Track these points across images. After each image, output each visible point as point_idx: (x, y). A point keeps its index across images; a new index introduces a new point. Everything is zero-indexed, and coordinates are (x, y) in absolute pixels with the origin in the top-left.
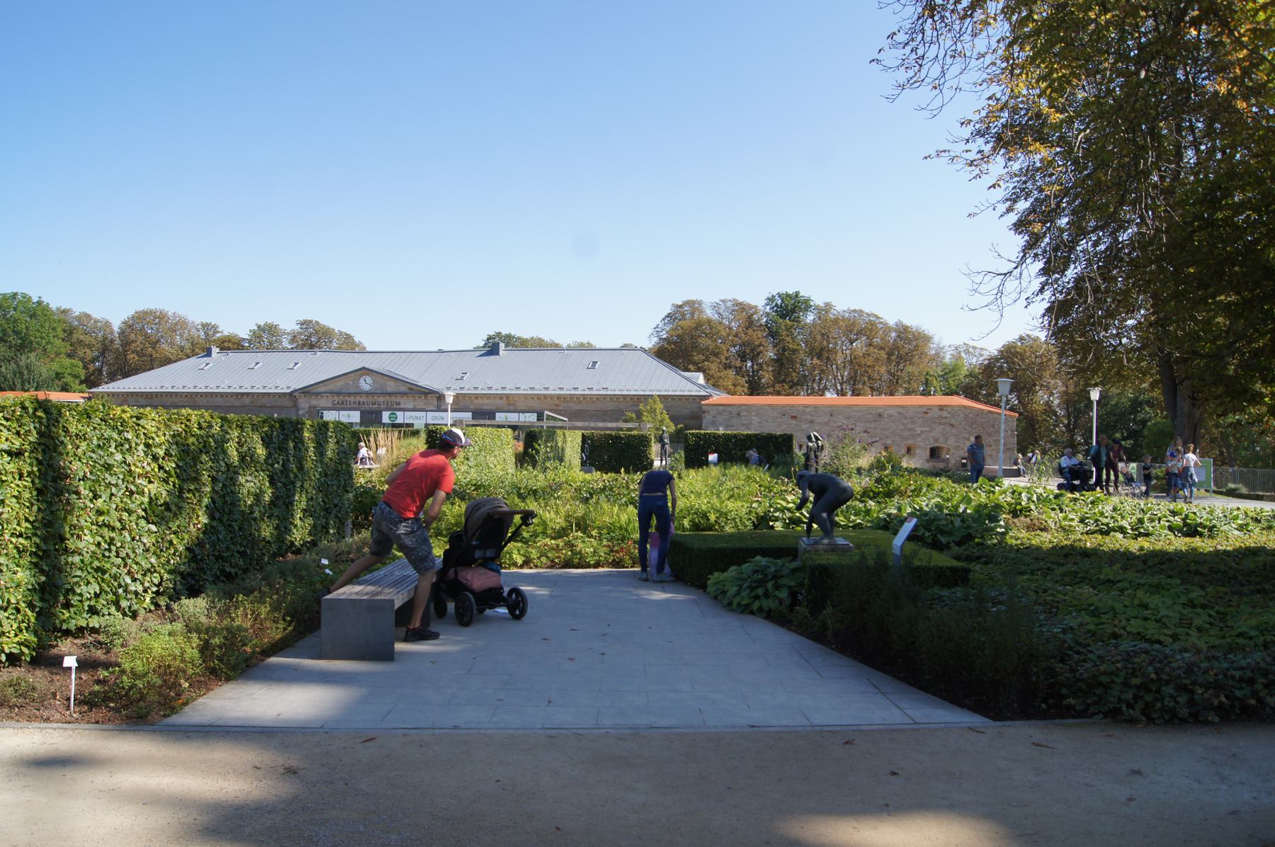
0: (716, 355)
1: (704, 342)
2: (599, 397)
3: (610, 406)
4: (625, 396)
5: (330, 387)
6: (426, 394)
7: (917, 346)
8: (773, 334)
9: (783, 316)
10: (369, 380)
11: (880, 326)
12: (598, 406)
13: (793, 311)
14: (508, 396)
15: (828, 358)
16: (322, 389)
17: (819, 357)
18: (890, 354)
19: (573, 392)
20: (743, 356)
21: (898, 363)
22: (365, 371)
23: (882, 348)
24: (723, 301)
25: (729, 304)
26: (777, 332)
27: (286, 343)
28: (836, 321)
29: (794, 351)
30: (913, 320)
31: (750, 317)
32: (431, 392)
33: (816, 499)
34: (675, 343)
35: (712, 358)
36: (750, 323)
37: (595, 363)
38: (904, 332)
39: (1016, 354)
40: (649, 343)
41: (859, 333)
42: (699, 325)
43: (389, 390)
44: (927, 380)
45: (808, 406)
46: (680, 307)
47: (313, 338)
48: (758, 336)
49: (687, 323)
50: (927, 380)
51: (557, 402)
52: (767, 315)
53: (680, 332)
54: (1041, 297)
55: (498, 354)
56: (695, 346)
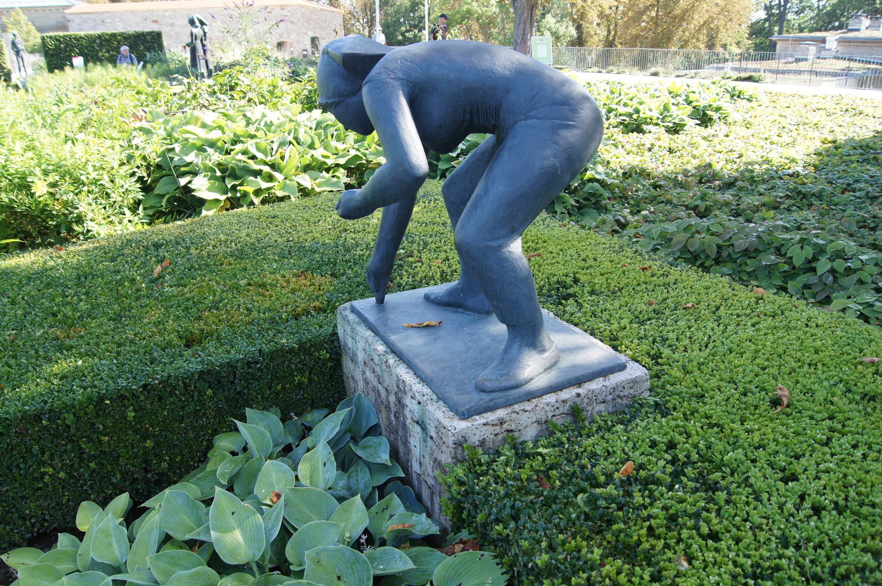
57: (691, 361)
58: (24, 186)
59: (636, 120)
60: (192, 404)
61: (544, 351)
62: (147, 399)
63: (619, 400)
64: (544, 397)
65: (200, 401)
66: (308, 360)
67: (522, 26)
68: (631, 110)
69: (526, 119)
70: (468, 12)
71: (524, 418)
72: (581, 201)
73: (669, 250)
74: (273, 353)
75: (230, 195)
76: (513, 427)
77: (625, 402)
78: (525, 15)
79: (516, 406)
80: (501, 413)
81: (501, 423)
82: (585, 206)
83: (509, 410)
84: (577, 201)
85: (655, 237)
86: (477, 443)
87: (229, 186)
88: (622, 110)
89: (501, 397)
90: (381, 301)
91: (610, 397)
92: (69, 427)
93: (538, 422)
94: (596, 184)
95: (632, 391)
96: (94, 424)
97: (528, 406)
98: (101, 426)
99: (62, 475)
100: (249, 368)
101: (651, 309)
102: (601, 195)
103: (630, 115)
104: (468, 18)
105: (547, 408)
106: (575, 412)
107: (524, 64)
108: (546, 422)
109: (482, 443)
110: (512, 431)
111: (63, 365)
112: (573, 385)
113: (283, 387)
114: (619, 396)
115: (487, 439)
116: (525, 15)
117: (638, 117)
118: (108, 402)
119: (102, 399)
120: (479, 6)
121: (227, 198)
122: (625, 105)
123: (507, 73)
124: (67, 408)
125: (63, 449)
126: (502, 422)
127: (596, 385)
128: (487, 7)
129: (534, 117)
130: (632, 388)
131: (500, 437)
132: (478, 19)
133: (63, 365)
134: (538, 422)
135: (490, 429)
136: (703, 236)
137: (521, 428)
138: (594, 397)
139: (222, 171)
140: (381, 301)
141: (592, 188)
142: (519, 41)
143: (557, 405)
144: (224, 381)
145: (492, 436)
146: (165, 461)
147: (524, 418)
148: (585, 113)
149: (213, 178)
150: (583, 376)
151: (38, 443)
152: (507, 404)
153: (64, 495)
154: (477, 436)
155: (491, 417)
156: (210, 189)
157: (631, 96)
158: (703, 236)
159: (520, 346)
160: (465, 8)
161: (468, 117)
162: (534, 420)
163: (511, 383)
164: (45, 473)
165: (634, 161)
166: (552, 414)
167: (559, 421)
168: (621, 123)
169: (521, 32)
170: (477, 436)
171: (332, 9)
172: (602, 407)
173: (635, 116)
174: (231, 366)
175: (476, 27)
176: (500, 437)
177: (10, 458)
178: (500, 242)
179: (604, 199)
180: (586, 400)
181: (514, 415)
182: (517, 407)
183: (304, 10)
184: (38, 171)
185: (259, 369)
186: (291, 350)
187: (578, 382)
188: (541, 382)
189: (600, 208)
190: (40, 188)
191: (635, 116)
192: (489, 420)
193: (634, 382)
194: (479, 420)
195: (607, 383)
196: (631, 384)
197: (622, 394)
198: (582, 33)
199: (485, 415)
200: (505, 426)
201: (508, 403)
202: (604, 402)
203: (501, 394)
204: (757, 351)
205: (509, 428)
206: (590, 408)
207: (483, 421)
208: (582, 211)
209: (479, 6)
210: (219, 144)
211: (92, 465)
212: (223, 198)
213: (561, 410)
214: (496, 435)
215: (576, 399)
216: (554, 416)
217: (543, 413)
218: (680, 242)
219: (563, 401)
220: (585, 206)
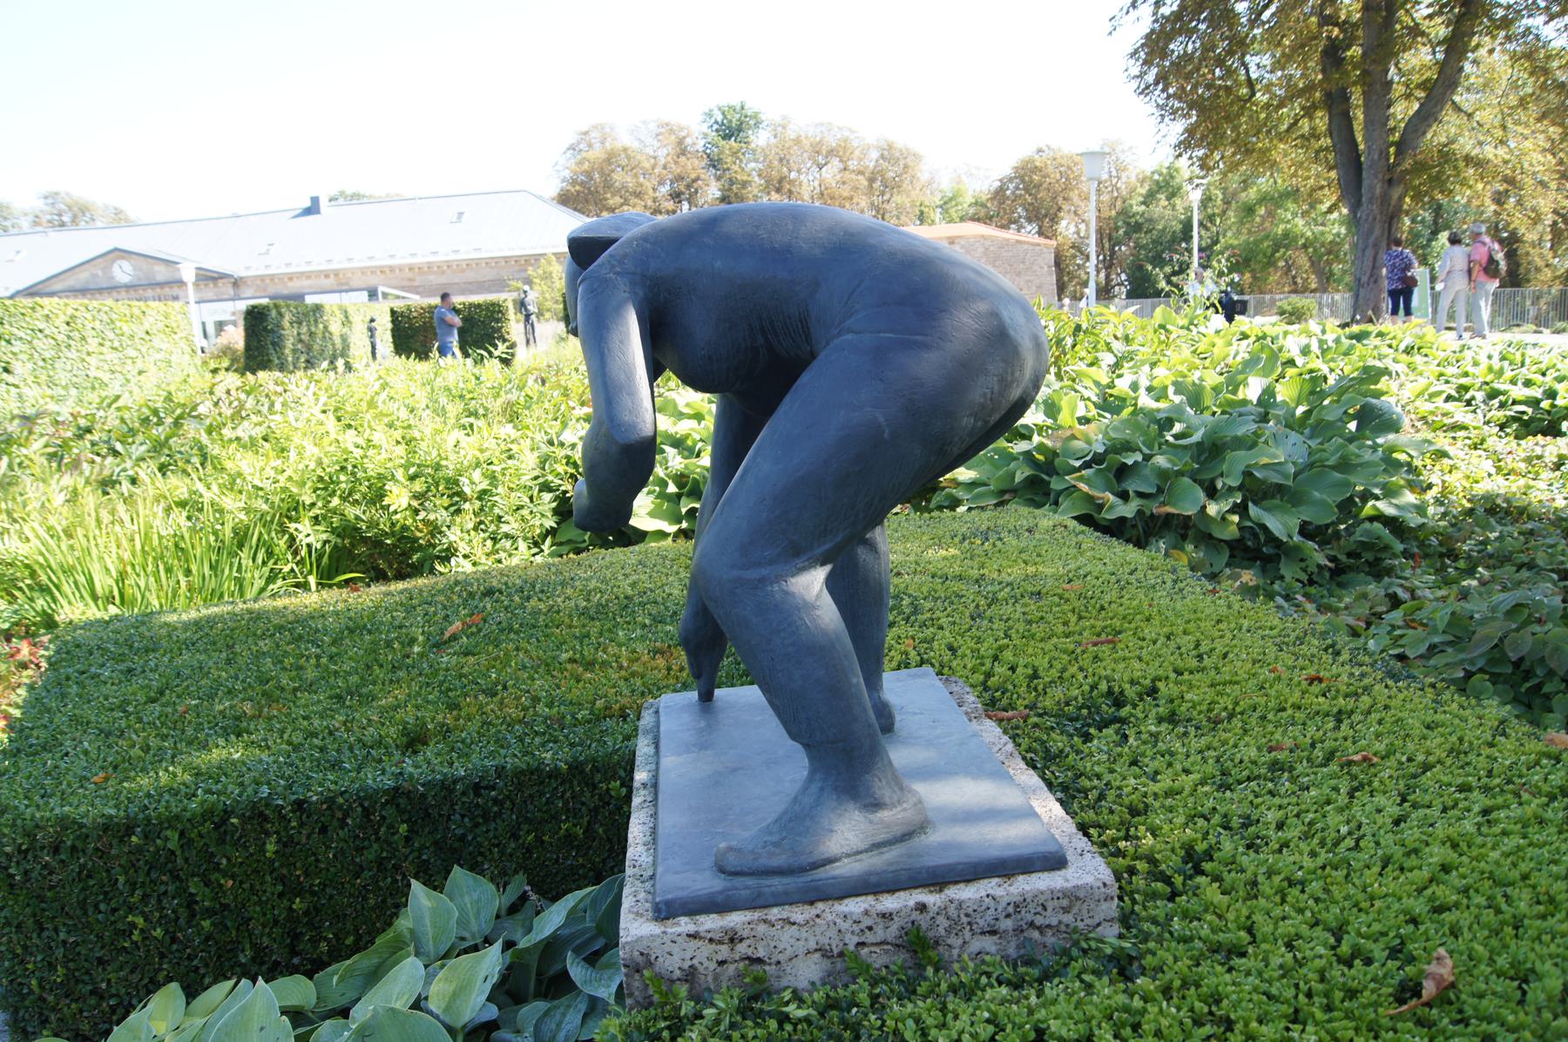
0: (638, 195)
1: (619, 177)
2: (469, 264)
3: (487, 274)
4: (507, 259)
5: (71, 282)
6: (214, 279)
7: (906, 166)
8: (714, 163)
9: (726, 137)
10: (126, 265)
11: (855, 144)
12: (470, 276)
13: (740, 130)
14: (336, 273)
15: (790, 191)
16: (57, 287)
17: (778, 190)
18: (871, 180)
19: (432, 259)
20: (676, 196)
21: (883, 193)
22: (119, 253)
23: (860, 173)
24: (644, 122)
25: (652, 126)
26: (719, 160)
27: (25, 224)
28: (797, 141)
29: (745, 184)
30: (902, 139)
31: (681, 142)
32: (223, 276)
33: (734, 440)
34: (582, 184)
35: (633, 200)
36: (682, 151)
37: (461, 214)
38: (889, 154)
39: (1036, 169)
40: (554, 187)
41: (831, 152)
42: (610, 158)
43: (160, 278)
44: (922, 213)
45: (479, 306)
46: (586, 133)
47: (67, 215)
48: (694, 166)
49: (597, 153)
50: (922, 213)
51: (410, 275)
52: (705, 136)
53: (586, 166)
54: (1133, 14)
55: (318, 212)
56: (608, 185)
57: (1270, 874)
58: (377, 496)
59: (1549, 412)
60: (375, 846)
61: (876, 805)
62: (302, 825)
63: (1036, 935)
64: (846, 901)
65: (389, 844)
66: (588, 795)
67: (1370, 252)
68: (1536, 393)
69: (839, 335)
70: (1286, 235)
71: (786, 938)
72: (1343, 558)
73: (1462, 656)
74: (522, 772)
75: (684, 525)
76: (761, 953)
77: (1050, 939)
78: (1377, 232)
79: (775, 910)
80: (736, 919)
81: (732, 940)
82: (1350, 568)
83: (757, 915)
84: (1333, 559)
85: (1441, 626)
86: (678, 973)
87: (684, 510)
88: (1519, 392)
89: (747, 888)
90: (707, 697)
91: (1007, 924)
92: (173, 853)
93: (824, 952)
94: (1377, 525)
95: (1068, 918)
96: (213, 855)
97: (799, 914)
98: (224, 861)
99: (158, 932)
100: (477, 794)
101: (1268, 757)
102: (1387, 548)
103: (1535, 403)
104: (1287, 247)
105: (845, 926)
106: (918, 945)
107: (852, 235)
108: (841, 954)
109: (690, 975)
110: (759, 961)
111: (223, 752)
112: (916, 887)
113: (539, 840)
114: (1031, 924)
115: (701, 969)
116: (1377, 232)
117: (1553, 406)
118: (234, 821)
119: (228, 813)
120: (1308, 223)
121: (680, 530)
122: (1528, 383)
123: (817, 251)
124: (172, 821)
125: (163, 889)
126: (733, 938)
127: (967, 893)
128: (1323, 224)
129: (850, 331)
130: (1066, 910)
131: (731, 969)
132: (1305, 246)
133: (223, 752)
134: (824, 952)
135: (706, 949)
136: (1546, 628)
137: (781, 957)
138: (964, 919)
139: (680, 485)
140: (707, 697)
141: (1367, 532)
142: (1364, 279)
143: (867, 922)
144: (434, 812)
145: (713, 965)
146: (325, 939)
147: (786, 937)
148: (964, 325)
149: (663, 496)
150: (950, 868)
151: (126, 873)
152: (756, 903)
153: (161, 969)
154: (676, 958)
155: (711, 923)
156: (652, 514)
157: (1543, 367)
158: (1546, 628)
159: (822, 789)
160: (1280, 229)
161: (760, 340)
162: (812, 945)
163: (804, 860)
164: (133, 925)
165: (1498, 486)
166: (856, 939)
167: (877, 959)
168: (1515, 419)
169: (1368, 263)
170: (676, 958)
171: (1042, 241)
172: (988, 943)
173: (1545, 404)
174: (446, 787)
175: (1303, 261)
176: (731, 969)
177: (83, 889)
178: (764, 572)
179: (1394, 556)
180: (943, 922)
181: (762, 928)
182: (775, 913)
183: (988, 243)
184: (400, 474)
185: (495, 801)
186: (555, 774)
187: (938, 879)
188: (847, 869)
189: (1378, 571)
190: (399, 497)
191: (1545, 404)
192: (702, 929)
193: (1072, 898)
194: (685, 925)
195: (999, 892)
196: (1065, 902)
197: (1039, 921)
198: (1518, 265)
199: (701, 918)
200: (742, 948)
201: (761, 902)
202: (993, 932)
203: (750, 881)
204: (1446, 869)
205: (750, 952)
206: (956, 941)
207: (691, 928)
208: (1343, 578)
209: (1308, 223)
210: (689, 442)
211: (206, 924)
212: (672, 529)
213: (880, 934)
214: (722, 963)
215: (916, 915)
216: (859, 944)
217: (832, 932)
218: (1487, 638)
219: (884, 916)
220: (1350, 568)
